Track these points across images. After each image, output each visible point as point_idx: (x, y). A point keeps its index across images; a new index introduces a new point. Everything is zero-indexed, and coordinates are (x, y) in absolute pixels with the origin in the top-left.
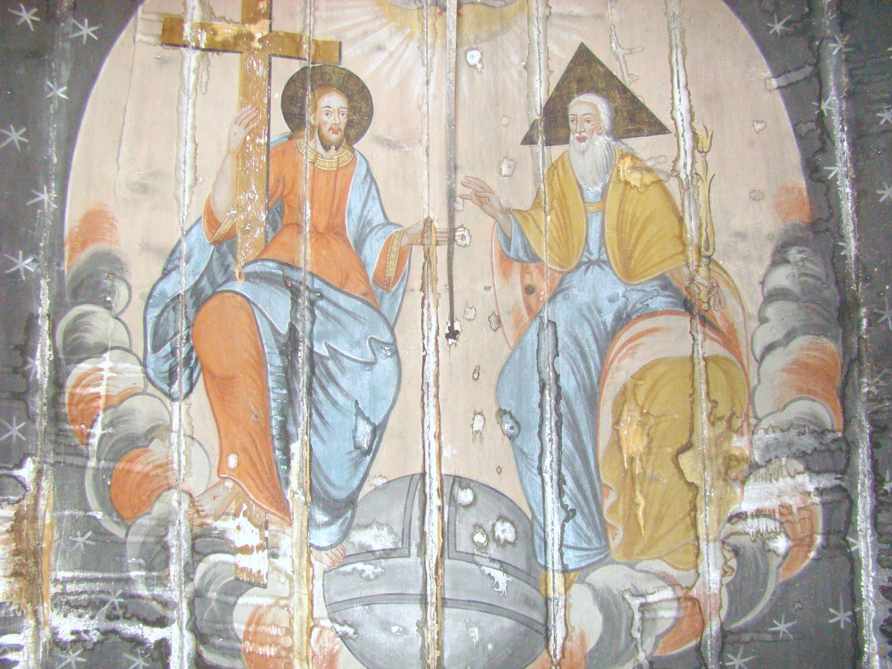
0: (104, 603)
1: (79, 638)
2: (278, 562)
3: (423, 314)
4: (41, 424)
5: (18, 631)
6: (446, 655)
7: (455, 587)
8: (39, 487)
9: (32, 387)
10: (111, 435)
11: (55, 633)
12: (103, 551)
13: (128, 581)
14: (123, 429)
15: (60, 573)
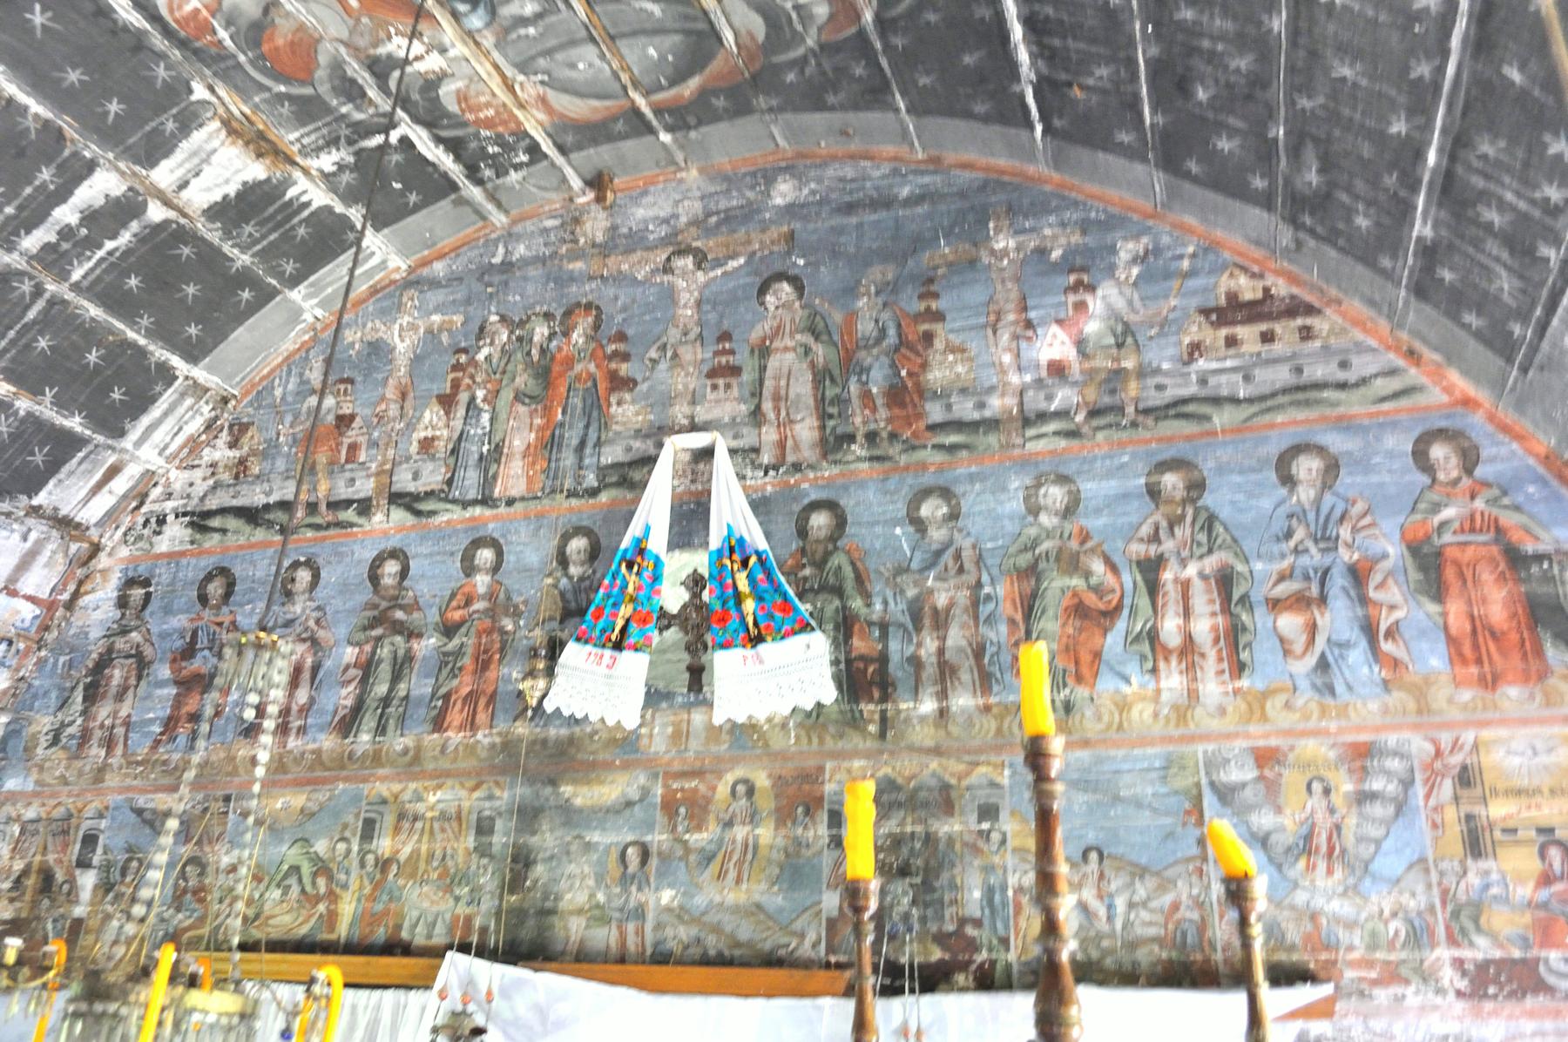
0: (338, 138)
1: (341, 167)
2: (452, 53)
3: (496, 67)
4: (176, 54)
5: (295, 183)
6: (636, 71)
7: (615, 24)
8: (219, 98)
9: (141, 34)
10: (238, 32)
11: (321, 171)
12: (307, 110)
13: (344, 116)
14: (243, 23)
15: (290, 138)
